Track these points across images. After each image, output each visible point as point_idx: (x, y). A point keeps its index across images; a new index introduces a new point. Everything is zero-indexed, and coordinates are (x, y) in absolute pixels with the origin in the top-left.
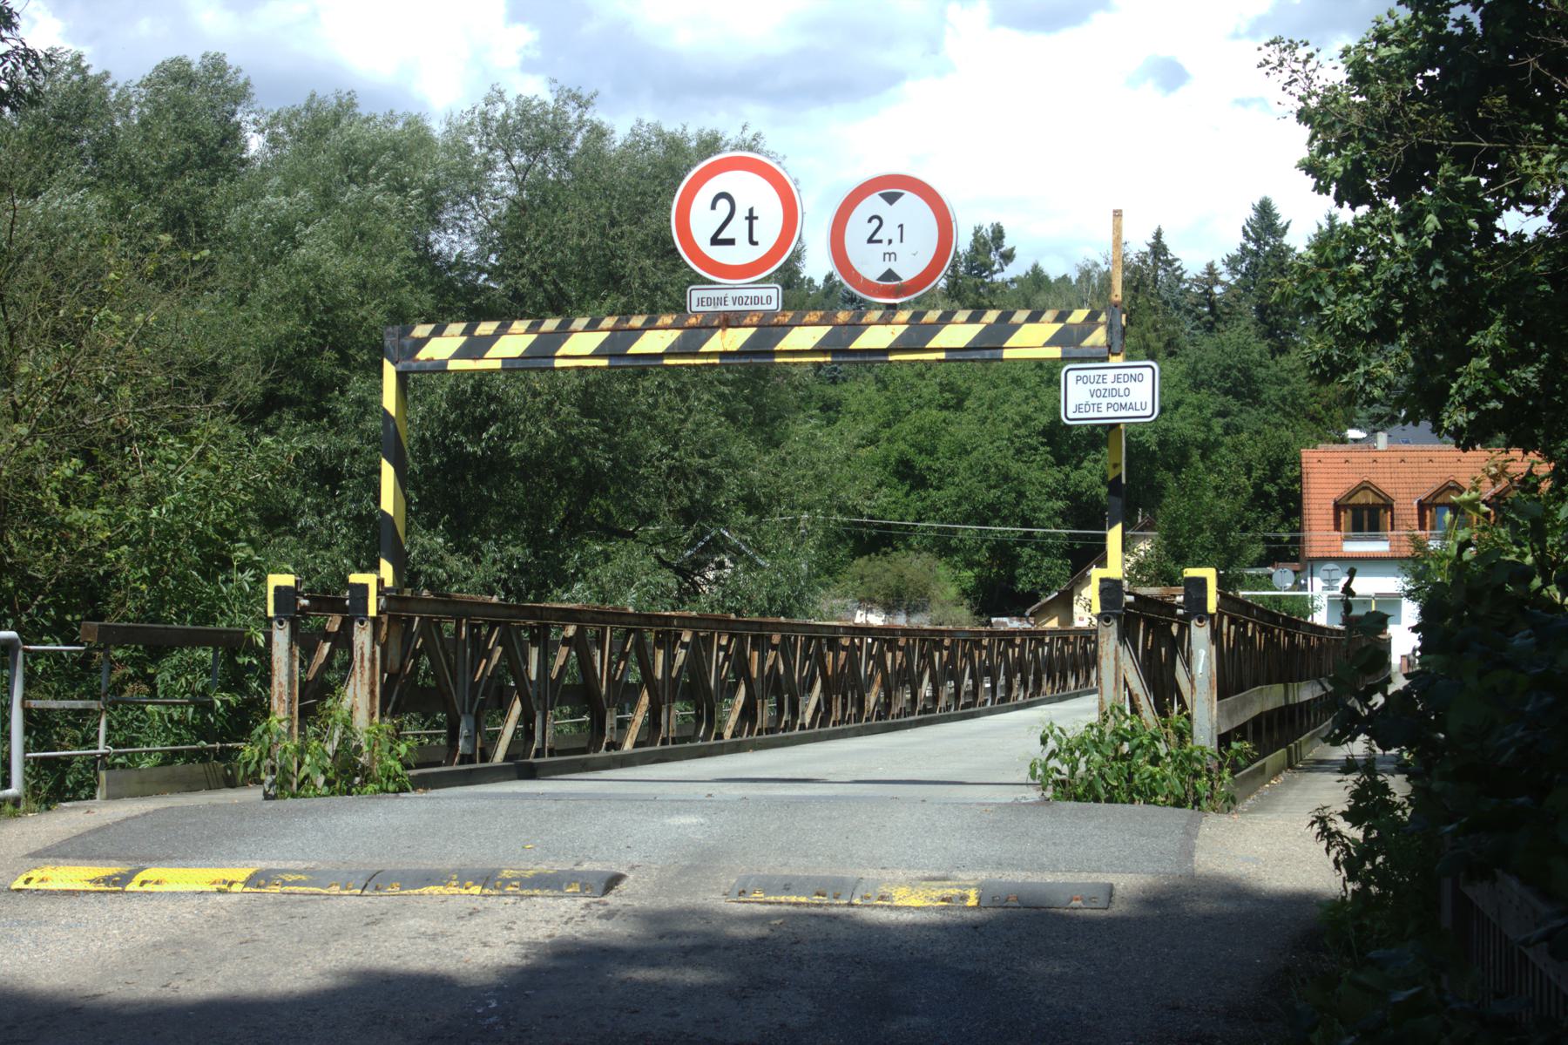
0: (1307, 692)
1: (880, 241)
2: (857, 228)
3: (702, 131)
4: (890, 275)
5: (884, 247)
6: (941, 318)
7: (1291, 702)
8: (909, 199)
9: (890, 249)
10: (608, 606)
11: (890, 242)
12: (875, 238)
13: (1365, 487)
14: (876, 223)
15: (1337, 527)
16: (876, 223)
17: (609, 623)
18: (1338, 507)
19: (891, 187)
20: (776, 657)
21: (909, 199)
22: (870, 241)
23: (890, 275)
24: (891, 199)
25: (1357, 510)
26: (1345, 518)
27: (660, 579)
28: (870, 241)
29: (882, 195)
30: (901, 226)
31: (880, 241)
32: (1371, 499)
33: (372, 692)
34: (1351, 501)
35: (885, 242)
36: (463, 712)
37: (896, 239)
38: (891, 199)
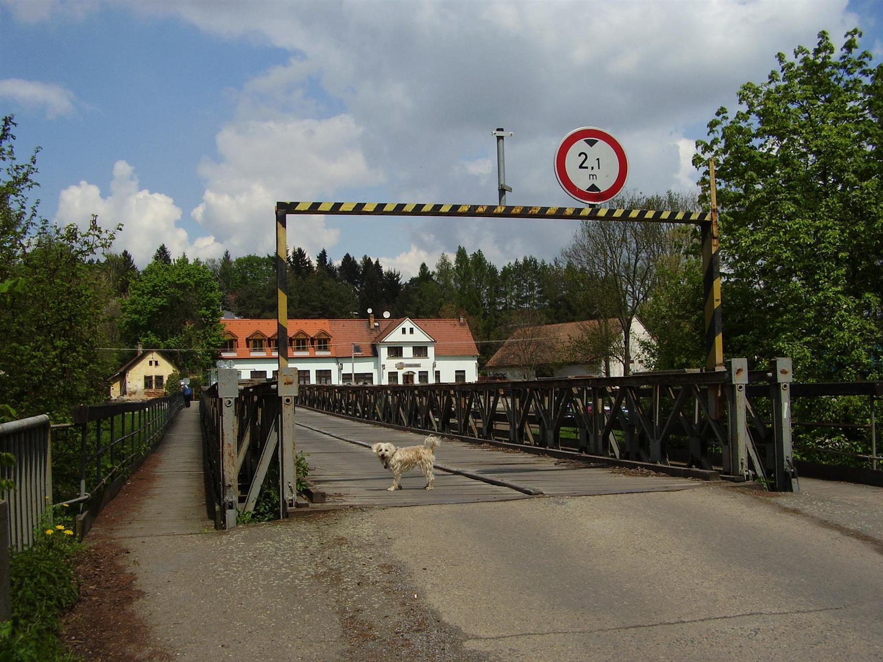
1: (587, 168)
3: (827, 34)
4: (593, 188)
5: (589, 171)
7: (560, 432)
8: (602, 147)
9: (593, 172)
12: (583, 166)
13: (257, 333)
14: (583, 156)
15: (248, 347)
16: (583, 156)
18: (248, 340)
19: (591, 136)
21: (601, 144)
22: (581, 167)
23: (593, 188)
24: (591, 143)
25: (255, 341)
26: (251, 343)
27: (863, 353)
28: (581, 167)
30: (598, 159)
31: (587, 168)
32: (260, 337)
34: (297, 337)
36: (548, 428)
38: (591, 143)
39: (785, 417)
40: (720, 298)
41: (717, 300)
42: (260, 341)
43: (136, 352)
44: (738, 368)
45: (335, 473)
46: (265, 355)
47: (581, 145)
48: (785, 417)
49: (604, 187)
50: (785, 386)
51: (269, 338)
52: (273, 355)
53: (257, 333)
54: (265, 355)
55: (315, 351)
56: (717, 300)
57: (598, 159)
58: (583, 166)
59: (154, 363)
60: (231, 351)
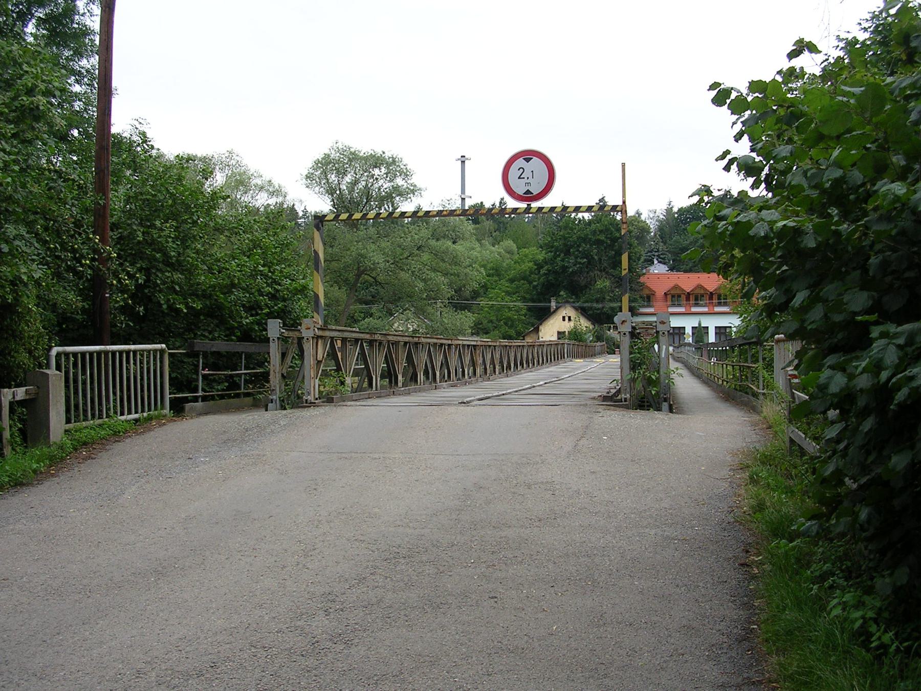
0: (833, 227)
2: (514, 173)
4: (528, 192)
5: (526, 180)
6: (413, 367)
10: (97, 67)
11: (528, 178)
12: (521, 177)
14: (522, 170)
16: (522, 170)
17: (108, 158)
19: (528, 155)
20: (809, 325)
22: (519, 178)
23: (528, 192)
24: (528, 160)
26: (669, 297)
28: (519, 178)
29: (524, 159)
30: (532, 171)
33: (451, 391)
35: (526, 178)
37: (530, 177)
38: (528, 160)
39: (663, 356)
40: (627, 268)
41: (625, 269)
42: (679, 296)
43: (549, 308)
44: (623, 319)
45: (422, 381)
46: (684, 310)
47: (520, 162)
48: (663, 356)
49: (535, 192)
50: (664, 333)
51: (711, 293)
52: (715, 310)
53: (676, 287)
54: (684, 310)
55: (691, 307)
56: (625, 269)
57: (532, 171)
58: (521, 177)
59: (567, 319)
60: (649, 306)
